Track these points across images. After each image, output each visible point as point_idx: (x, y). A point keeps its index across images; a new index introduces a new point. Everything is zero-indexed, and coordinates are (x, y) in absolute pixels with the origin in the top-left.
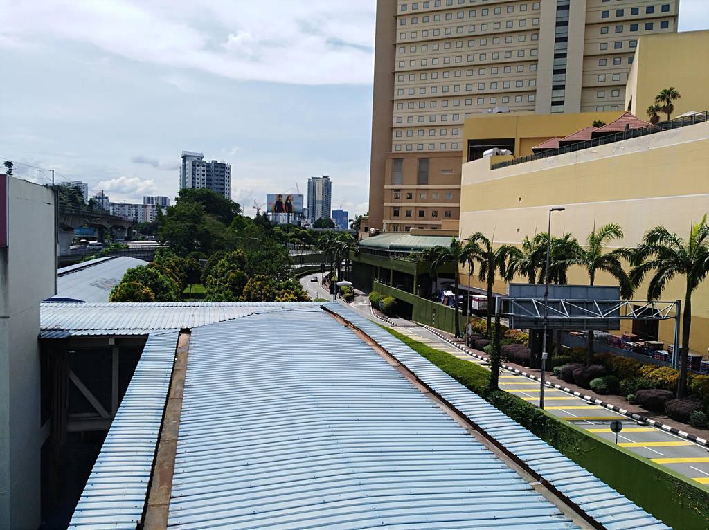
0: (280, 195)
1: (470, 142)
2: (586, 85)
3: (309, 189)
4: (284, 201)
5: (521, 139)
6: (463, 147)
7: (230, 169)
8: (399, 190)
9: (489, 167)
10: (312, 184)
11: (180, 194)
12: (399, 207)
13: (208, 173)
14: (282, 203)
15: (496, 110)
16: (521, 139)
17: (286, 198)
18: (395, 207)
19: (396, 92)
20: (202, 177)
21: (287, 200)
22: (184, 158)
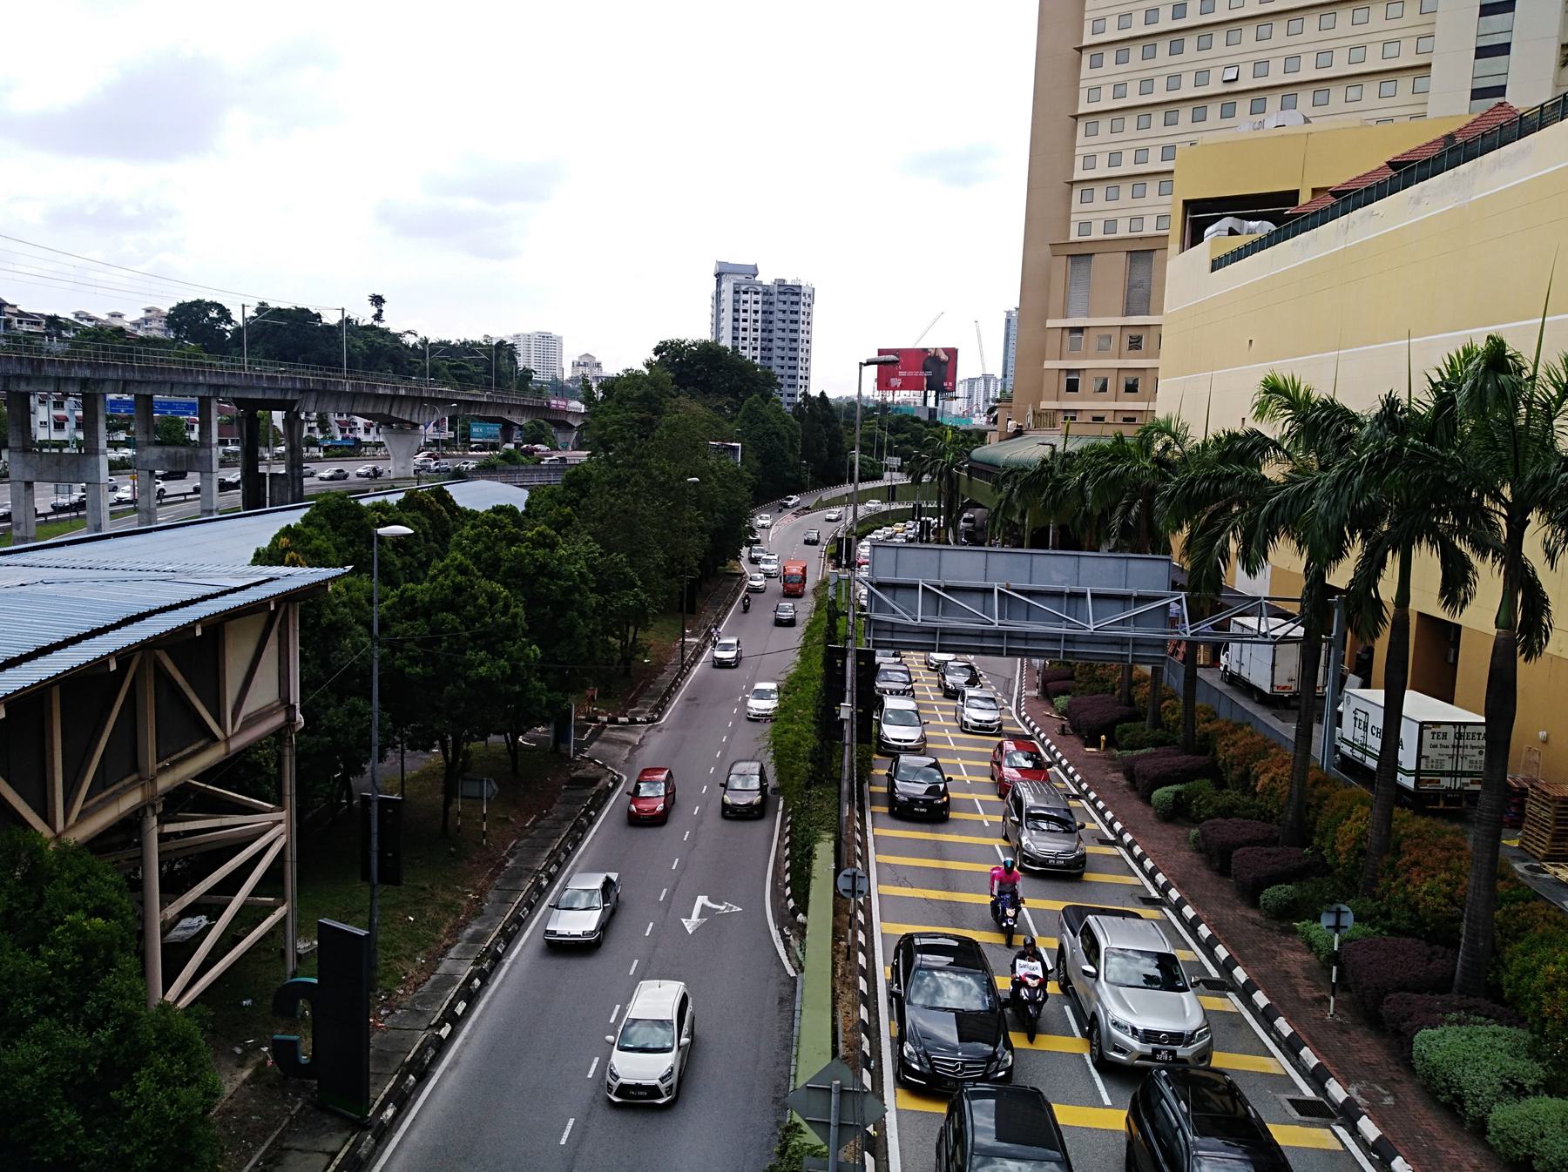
1: (1187, 204)
3: (1007, 335)
5: (1315, 191)
7: (811, 296)
8: (1080, 330)
9: (1208, 266)
12: (1078, 371)
13: (766, 307)
15: (1271, 123)
16: (1315, 191)
18: (1069, 371)
20: (753, 315)
22: (718, 275)
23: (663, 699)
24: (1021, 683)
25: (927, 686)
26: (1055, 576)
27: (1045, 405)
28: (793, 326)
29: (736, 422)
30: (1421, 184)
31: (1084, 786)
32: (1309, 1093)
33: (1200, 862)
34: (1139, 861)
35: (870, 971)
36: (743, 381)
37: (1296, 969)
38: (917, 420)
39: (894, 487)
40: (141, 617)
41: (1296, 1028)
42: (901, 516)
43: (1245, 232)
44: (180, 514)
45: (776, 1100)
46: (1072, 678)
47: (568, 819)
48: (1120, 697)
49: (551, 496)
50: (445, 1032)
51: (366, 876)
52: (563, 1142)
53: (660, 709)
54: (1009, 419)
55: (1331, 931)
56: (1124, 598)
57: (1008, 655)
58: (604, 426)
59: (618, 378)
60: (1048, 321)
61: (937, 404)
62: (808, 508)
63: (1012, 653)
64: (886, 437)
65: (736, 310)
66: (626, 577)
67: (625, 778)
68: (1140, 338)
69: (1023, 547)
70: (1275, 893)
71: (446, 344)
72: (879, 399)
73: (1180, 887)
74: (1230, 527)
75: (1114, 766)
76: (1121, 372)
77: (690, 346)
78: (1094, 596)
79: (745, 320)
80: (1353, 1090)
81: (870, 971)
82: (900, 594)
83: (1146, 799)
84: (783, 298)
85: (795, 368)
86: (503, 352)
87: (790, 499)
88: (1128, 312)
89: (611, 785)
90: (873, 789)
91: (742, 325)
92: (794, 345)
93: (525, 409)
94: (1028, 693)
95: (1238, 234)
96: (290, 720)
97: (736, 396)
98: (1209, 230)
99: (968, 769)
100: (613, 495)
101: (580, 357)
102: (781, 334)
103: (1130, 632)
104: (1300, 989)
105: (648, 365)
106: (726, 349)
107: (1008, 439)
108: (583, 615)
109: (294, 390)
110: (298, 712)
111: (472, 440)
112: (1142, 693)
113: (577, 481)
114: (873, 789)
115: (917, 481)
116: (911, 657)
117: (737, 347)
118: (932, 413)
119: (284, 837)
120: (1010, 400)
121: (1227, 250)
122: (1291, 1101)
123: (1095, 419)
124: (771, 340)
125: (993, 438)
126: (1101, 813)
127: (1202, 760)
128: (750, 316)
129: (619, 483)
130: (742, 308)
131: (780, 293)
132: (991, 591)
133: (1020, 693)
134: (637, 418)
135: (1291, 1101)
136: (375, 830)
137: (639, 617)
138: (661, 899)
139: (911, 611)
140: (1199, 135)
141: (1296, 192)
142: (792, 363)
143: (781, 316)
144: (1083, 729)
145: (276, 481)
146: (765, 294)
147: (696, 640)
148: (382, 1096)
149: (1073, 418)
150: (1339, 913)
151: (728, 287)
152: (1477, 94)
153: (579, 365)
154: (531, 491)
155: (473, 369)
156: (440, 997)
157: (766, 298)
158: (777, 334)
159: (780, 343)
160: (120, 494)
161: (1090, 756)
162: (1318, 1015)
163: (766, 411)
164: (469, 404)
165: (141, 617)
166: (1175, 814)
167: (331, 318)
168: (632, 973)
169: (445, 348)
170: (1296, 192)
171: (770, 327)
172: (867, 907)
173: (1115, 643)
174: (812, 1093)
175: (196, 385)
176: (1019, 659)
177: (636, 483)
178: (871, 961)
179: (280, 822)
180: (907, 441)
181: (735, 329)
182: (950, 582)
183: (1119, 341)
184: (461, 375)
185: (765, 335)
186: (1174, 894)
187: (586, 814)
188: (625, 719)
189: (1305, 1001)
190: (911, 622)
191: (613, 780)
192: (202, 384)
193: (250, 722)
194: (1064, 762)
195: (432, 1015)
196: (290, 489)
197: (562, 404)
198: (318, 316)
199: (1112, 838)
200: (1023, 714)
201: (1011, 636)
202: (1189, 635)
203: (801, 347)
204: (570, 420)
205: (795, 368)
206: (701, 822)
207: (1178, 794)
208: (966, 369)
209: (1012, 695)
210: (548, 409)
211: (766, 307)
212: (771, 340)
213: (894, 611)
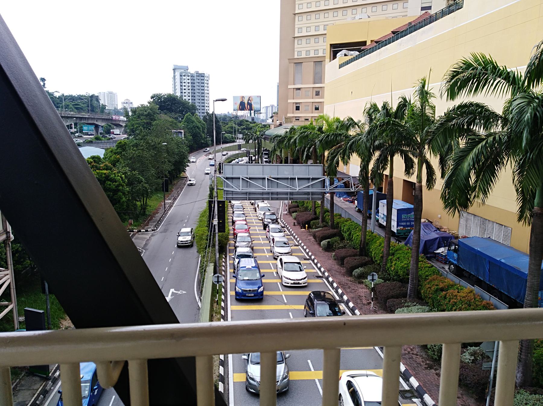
0: (243, 97)
1: (331, 45)
4: (246, 101)
5: (372, 41)
6: (324, 50)
7: (208, 77)
8: (299, 89)
11: (59, 96)
13: (192, 81)
15: (358, 17)
16: (372, 41)
17: (248, 99)
18: (296, 103)
20: (188, 84)
21: (248, 100)
22: (174, 70)
23: (158, 223)
24: (282, 209)
26: (286, 173)
28: (202, 88)
29: (182, 123)
30: (401, 39)
31: (300, 242)
33: (336, 263)
34: (316, 265)
35: (226, 308)
36: (184, 108)
38: (247, 121)
39: (240, 145)
41: (361, 313)
42: (242, 155)
43: (350, 55)
46: (298, 206)
49: (111, 152)
51: (44, 292)
53: (157, 226)
54: (277, 120)
55: (371, 281)
56: (308, 179)
57: (271, 200)
58: (133, 125)
59: (138, 108)
60: (289, 86)
61: (254, 115)
62: (210, 153)
64: (237, 127)
65: (181, 82)
66: (138, 179)
67: (144, 251)
68: (319, 92)
69: (288, 163)
71: (71, 96)
72: (235, 114)
74: (339, 153)
76: (313, 103)
77: (164, 95)
78: (298, 179)
81: (226, 308)
84: (198, 78)
85: (204, 103)
86: (94, 98)
87: (207, 149)
88: (315, 83)
90: (230, 248)
91: (184, 88)
92: (203, 95)
93: (103, 120)
94: (284, 213)
95: (347, 56)
96: (8, 237)
97: (182, 114)
98: (338, 54)
99: (259, 240)
100: (135, 150)
102: (198, 91)
103: (310, 190)
104: (363, 300)
105: (149, 103)
106: (177, 96)
107: (277, 127)
108: (124, 194)
110: (11, 233)
111: (83, 132)
113: (122, 146)
114: (230, 248)
115: (247, 142)
116: (246, 203)
117: (182, 96)
118: (253, 119)
123: (306, 120)
124: (195, 93)
125: (272, 127)
126: (305, 250)
128: (187, 84)
129: (136, 145)
130: (183, 81)
131: (197, 76)
132: (264, 178)
133: (281, 213)
134: (145, 122)
137: (145, 194)
139: (238, 187)
142: (203, 101)
143: (198, 84)
146: (191, 76)
147: (170, 201)
148: (55, 368)
149: (299, 120)
150: (373, 275)
151: (178, 74)
153: (124, 103)
154: (106, 150)
155: (82, 105)
158: (197, 91)
159: (198, 94)
161: (303, 232)
162: (368, 308)
163: (193, 119)
164: (81, 118)
166: (328, 248)
169: (72, 98)
172: (226, 287)
176: (282, 201)
177: (142, 146)
179: (8, 274)
180: (244, 129)
181: (181, 89)
183: (312, 93)
184: (78, 108)
185: (192, 91)
186: (326, 274)
188: (144, 230)
190: (238, 190)
197: (117, 118)
199: (308, 258)
200: (282, 219)
201: (272, 193)
202: (328, 190)
203: (206, 95)
204: (121, 124)
205: (204, 103)
206: (172, 264)
207: (329, 242)
208: (264, 103)
209: (279, 214)
210: (112, 120)
212: (195, 93)
213: (233, 187)
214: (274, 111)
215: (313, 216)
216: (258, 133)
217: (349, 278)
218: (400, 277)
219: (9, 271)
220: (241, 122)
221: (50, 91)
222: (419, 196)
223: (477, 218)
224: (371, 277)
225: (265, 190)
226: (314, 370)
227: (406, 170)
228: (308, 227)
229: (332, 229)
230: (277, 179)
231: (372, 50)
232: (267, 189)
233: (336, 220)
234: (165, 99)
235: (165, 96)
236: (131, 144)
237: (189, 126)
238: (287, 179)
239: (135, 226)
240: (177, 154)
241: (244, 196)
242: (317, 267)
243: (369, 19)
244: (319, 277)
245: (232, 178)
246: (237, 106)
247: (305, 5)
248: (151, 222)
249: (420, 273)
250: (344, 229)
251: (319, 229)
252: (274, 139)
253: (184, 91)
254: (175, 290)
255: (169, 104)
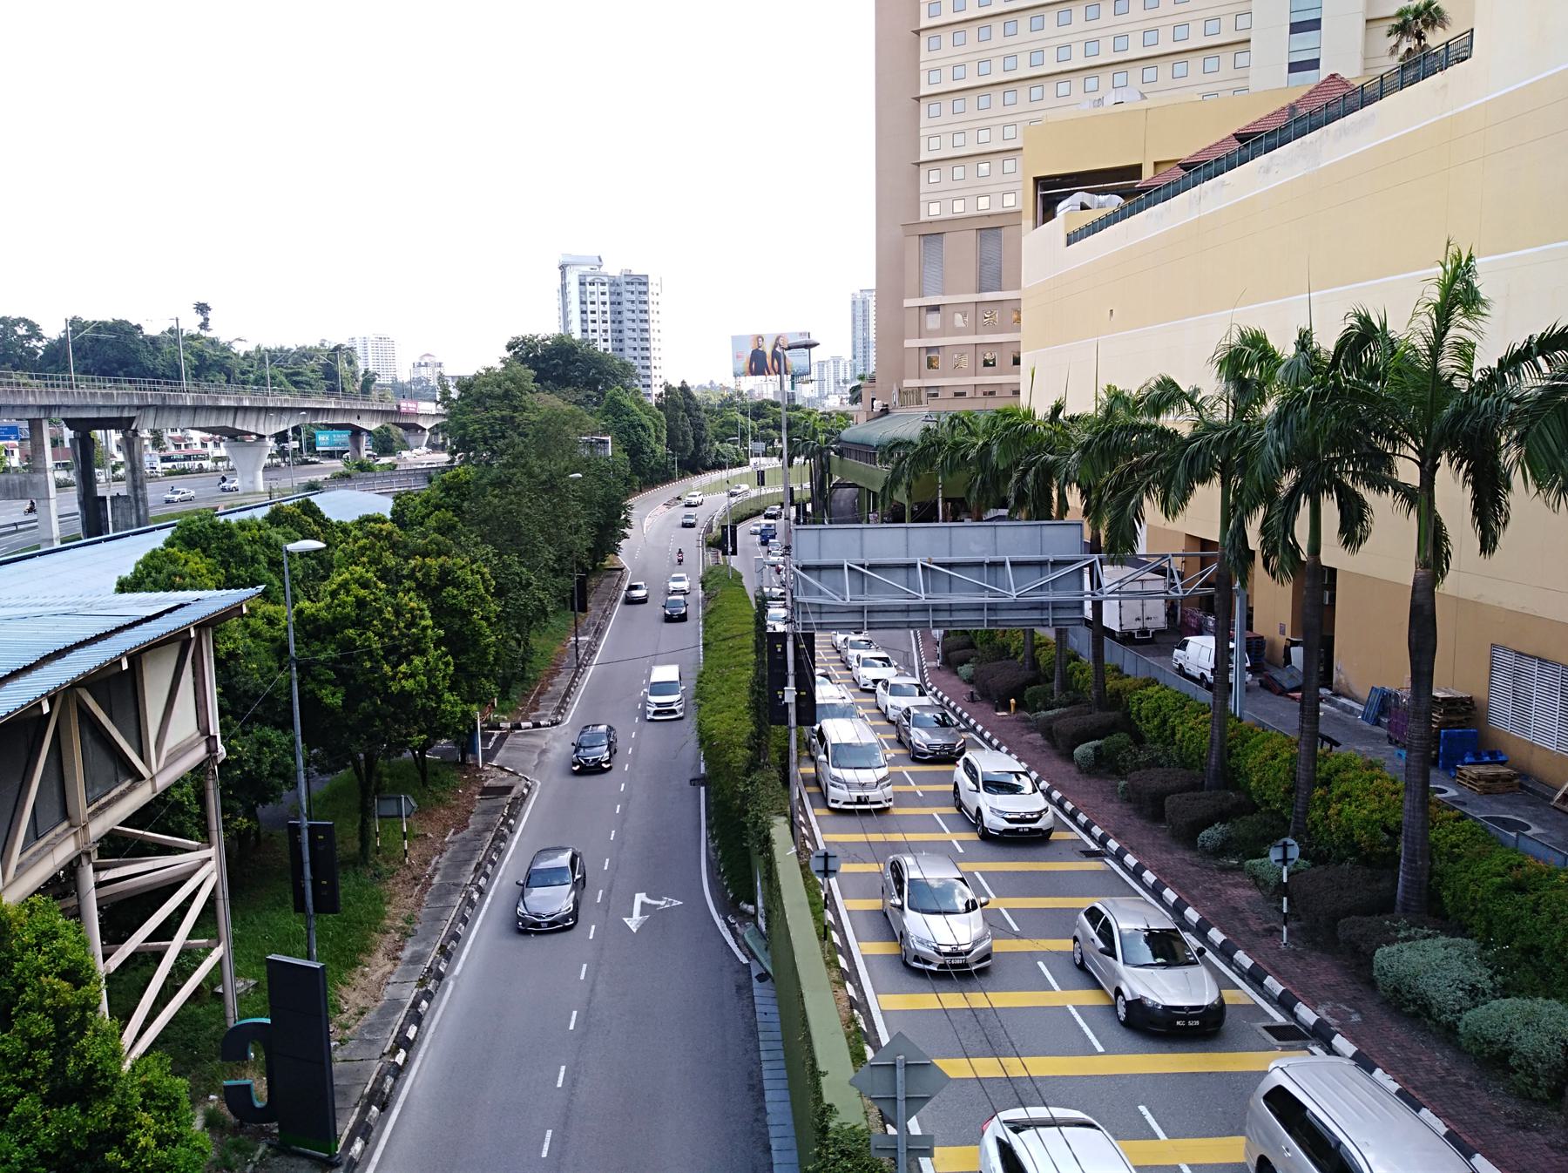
0: (760, 337)
2: (1370, 17)
5: (1156, 164)
6: (1020, 198)
9: (1064, 239)
10: (859, 304)
12: (937, 348)
13: (614, 298)
14: (764, 353)
15: (1110, 99)
16: (1156, 164)
18: (929, 349)
19: (924, 77)
22: (563, 268)
23: (564, 701)
24: (919, 655)
25: (831, 666)
26: (975, 548)
27: (909, 383)
32: (1280, 1019)
33: (1131, 812)
37: (1243, 904)
40: (59, 654)
44: (10, 547)
45: (752, 1087)
46: (971, 645)
47: (487, 829)
48: (1023, 662)
50: (400, 1058)
52: (544, 1154)
55: (1279, 864)
61: (793, 388)
63: (910, 625)
65: (583, 303)
67: (539, 783)
69: (937, 521)
70: (1212, 835)
73: (1117, 837)
75: (1028, 728)
78: (1012, 564)
79: (593, 312)
80: (1322, 1011)
82: (825, 574)
83: (1068, 757)
84: (630, 288)
89: (525, 791)
91: (591, 317)
94: (929, 664)
96: (211, 750)
98: (1060, 206)
100: (496, 496)
101: (422, 357)
103: (1049, 597)
109: (130, 407)
112: (1044, 657)
118: (791, 398)
119: (215, 875)
120: (873, 380)
121: (1082, 224)
122: (1266, 1028)
123: (957, 394)
127: (1113, 715)
128: (598, 308)
130: (589, 300)
131: (628, 283)
132: (914, 566)
133: (921, 666)
135: (1266, 1028)
136: (307, 857)
138: (599, 900)
140: (1048, 112)
141: (1140, 166)
144: (989, 694)
145: (120, 502)
149: (936, 395)
150: (1285, 846)
152: (1294, 67)
153: (420, 365)
156: (389, 1023)
157: (613, 289)
160: (902, 489)
165: (59, 654)
166: (1102, 766)
167: (152, 329)
168: (582, 977)
169: (277, 357)
170: (1140, 166)
171: (619, 318)
173: (1036, 609)
174: (876, 1070)
175: (25, 407)
178: (844, 938)
179: (210, 859)
181: (584, 321)
182: (875, 561)
185: (615, 326)
186: (1113, 845)
187: (505, 823)
189: (1256, 934)
190: (840, 602)
191: (527, 786)
192: (33, 406)
193: (174, 757)
194: (979, 728)
195: (383, 1042)
196: (135, 513)
198: (139, 327)
204: (421, 423)
207: (1097, 748)
211: (614, 298)
213: (820, 592)
214: (859, 372)
215: (1030, 674)
216: (822, 437)
217: (1187, 856)
218: (1361, 849)
219: (213, 849)
220: (758, 408)
221: (223, 340)
222: (1427, 607)
223: (1549, 669)
224: (1280, 850)
225: (917, 598)
226: (1167, 1135)
227: (1342, 531)
228: (1016, 706)
229: (1101, 709)
230: (950, 566)
231: (1173, 190)
232: (923, 598)
233: (1111, 684)
234: (547, 349)
235: (548, 342)
236: (485, 481)
237: (619, 425)
238: (980, 564)
239: (503, 712)
240: (601, 505)
241: (856, 618)
242: (1078, 826)
243: (1145, 104)
244: (1090, 854)
245: (819, 568)
246: (744, 363)
247: (947, 73)
248: (545, 700)
249: (1433, 835)
250: (1139, 710)
251: (1056, 711)
252: (890, 450)
253: (591, 326)
254: (648, 896)
255: (557, 364)
